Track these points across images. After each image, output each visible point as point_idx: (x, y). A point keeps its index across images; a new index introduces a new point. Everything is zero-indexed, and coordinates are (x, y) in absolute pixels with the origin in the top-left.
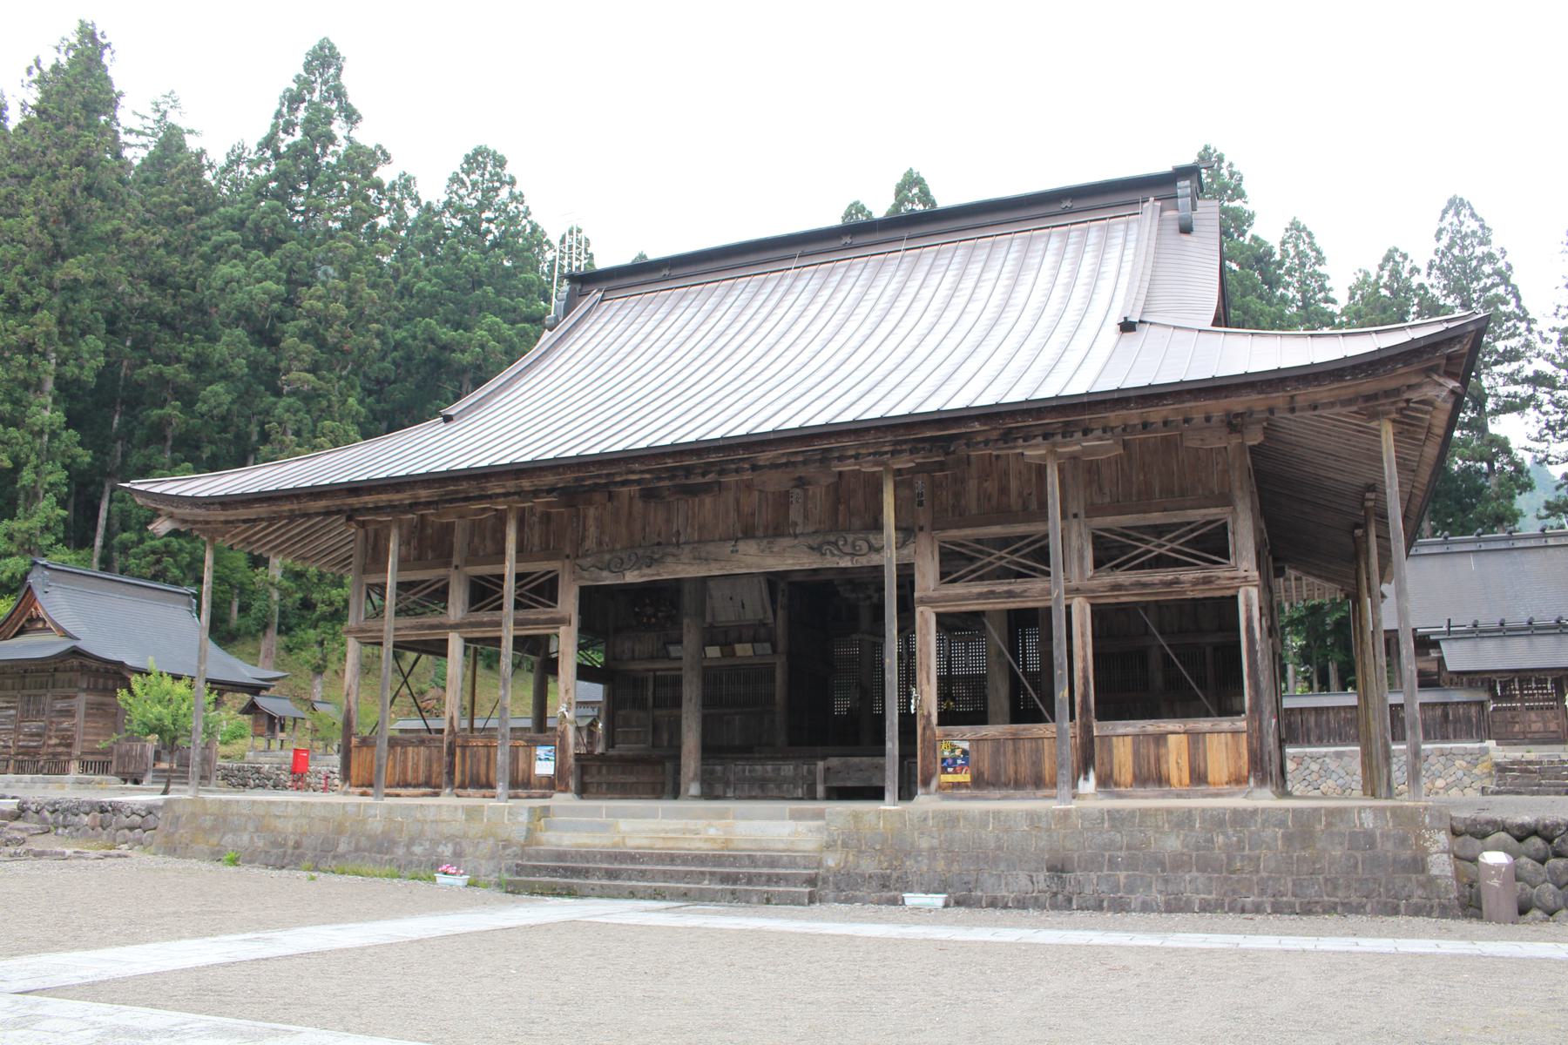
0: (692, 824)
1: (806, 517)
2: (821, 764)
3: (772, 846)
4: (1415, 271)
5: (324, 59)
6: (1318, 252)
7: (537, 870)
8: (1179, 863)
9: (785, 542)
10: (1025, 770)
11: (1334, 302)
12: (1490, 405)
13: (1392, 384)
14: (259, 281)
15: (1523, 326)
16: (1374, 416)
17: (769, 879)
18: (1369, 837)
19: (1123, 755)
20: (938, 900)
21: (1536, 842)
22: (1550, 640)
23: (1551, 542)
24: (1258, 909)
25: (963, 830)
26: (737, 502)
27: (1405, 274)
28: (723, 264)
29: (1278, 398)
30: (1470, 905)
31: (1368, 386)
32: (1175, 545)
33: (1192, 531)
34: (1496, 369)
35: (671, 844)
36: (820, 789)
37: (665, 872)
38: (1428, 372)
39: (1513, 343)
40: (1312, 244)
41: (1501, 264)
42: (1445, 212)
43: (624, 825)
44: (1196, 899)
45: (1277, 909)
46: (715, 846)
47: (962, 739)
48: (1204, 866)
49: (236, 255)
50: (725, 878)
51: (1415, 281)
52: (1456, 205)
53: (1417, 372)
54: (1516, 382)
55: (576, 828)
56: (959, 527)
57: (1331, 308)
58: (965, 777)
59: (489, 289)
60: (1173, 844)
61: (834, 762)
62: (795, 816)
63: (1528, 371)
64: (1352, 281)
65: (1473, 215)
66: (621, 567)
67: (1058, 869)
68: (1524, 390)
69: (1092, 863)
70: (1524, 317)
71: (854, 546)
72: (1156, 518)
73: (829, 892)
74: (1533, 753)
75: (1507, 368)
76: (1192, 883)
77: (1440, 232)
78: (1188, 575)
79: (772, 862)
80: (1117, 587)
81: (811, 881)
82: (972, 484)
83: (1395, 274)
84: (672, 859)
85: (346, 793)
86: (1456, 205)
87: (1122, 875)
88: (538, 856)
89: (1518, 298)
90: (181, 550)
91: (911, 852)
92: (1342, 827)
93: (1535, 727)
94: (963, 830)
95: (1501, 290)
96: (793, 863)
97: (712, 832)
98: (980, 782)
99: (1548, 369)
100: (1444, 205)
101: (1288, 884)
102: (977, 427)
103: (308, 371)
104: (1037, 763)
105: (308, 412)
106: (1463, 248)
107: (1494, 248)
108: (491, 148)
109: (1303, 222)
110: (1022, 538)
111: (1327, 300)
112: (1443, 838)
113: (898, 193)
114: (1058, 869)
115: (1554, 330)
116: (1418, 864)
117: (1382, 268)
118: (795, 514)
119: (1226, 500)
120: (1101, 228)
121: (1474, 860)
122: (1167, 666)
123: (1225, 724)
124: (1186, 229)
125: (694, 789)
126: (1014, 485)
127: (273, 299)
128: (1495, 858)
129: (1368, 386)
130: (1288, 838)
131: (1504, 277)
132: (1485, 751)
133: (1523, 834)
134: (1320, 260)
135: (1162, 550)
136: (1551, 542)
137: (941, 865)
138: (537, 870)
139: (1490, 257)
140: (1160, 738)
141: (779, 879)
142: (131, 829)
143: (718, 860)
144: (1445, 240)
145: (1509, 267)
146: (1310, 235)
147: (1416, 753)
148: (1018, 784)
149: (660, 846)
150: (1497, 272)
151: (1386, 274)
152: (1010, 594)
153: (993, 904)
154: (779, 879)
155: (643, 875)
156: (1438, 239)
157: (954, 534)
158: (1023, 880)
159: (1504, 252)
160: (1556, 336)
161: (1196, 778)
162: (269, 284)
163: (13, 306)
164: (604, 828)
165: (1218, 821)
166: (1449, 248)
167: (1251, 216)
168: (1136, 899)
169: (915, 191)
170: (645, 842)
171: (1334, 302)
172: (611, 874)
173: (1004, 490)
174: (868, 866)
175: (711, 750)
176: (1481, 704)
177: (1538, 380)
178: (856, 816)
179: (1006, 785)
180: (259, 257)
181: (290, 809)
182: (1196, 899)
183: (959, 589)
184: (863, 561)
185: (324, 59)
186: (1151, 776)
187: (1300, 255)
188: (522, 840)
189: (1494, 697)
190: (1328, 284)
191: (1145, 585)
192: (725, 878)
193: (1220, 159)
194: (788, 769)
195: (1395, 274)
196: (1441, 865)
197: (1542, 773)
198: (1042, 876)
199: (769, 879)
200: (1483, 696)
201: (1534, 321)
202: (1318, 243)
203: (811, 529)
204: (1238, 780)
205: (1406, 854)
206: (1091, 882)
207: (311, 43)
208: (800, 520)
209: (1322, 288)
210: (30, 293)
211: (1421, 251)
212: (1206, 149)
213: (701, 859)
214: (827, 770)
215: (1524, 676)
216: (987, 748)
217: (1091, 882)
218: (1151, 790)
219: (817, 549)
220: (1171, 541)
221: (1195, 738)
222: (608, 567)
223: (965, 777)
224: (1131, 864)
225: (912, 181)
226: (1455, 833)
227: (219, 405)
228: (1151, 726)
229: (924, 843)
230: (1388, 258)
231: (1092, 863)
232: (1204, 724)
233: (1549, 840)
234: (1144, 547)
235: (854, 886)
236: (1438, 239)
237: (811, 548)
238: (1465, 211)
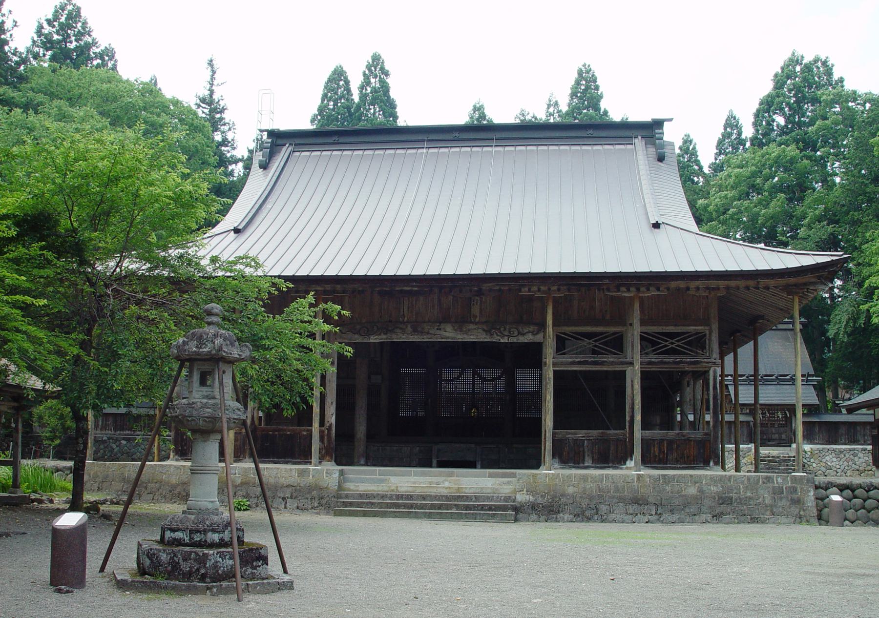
1: (481, 313)
3: (484, 491)
26: (439, 300)
28: (352, 139)
31: (793, 280)
32: (679, 344)
33: (689, 337)
35: (426, 490)
36: (435, 462)
37: (492, 501)
46: (452, 490)
53: (814, 277)
56: (567, 325)
62: (491, 476)
66: (368, 334)
71: (510, 332)
72: (671, 329)
85: (177, 460)
97: (447, 484)
102: (607, 281)
110: (602, 333)
118: (475, 310)
119: (706, 322)
122: (592, 418)
126: (597, 304)
129: (793, 280)
135: (673, 346)
147: (737, 450)
149: (418, 492)
155: (422, 507)
164: (382, 481)
170: (410, 489)
178: (534, 476)
181: (172, 469)
183: (567, 359)
184: (514, 340)
188: (336, 488)
191: (665, 363)
203: (483, 320)
208: (478, 314)
213: (448, 498)
220: (678, 341)
222: (358, 333)
225: (478, 109)
226: (817, 487)
233: (853, 491)
234: (679, 344)
237: (484, 330)
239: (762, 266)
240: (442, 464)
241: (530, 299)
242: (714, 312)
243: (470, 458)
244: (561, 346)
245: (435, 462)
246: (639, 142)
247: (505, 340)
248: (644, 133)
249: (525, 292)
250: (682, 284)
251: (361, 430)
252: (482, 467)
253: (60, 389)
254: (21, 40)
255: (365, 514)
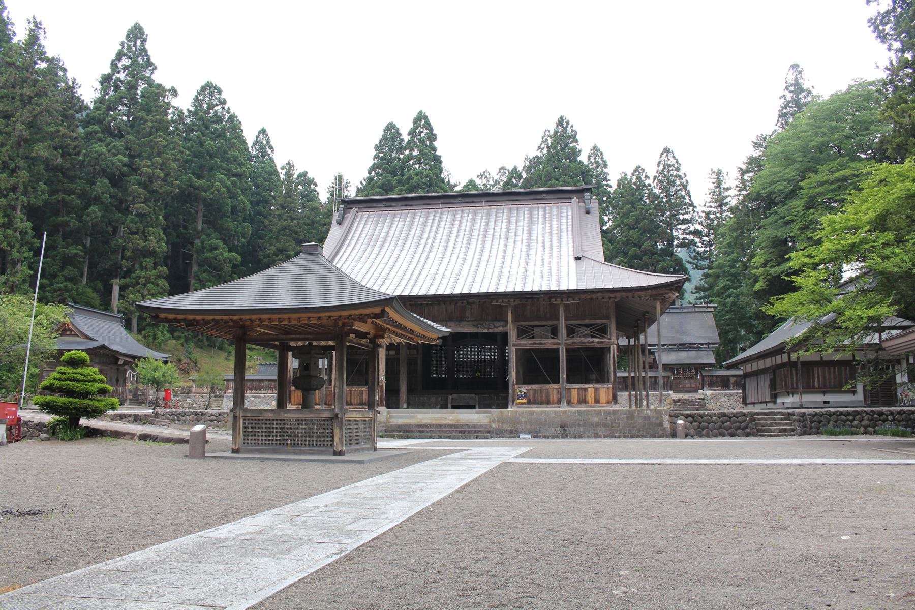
0: (444, 416)
2: (450, 397)
4: (647, 177)
5: (136, 33)
6: (605, 162)
7: (394, 431)
8: (598, 425)
9: (464, 323)
10: (544, 399)
11: (610, 187)
12: (675, 243)
13: (661, 292)
14: (115, 155)
15: (691, 208)
16: (655, 299)
17: (475, 431)
18: (649, 418)
19: (574, 394)
20: (530, 436)
21: (690, 418)
22: (694, 353)
23: (697, 310)
24: (619, 437)
25: (535, 416)
27: (643, 179)
29: (630, 295)
30: (674, 435)
31: (654, 292)
34: (679, 227)
36: (450, 406)
38: (671, 290)
39: (686, 217)
40: (602, 158)
41: (684, 180)
42: (662, 154)
43: (419, 416)
44: (602, 435)
45: (624, 437)
47: (524, 389)
48: (605, 425)
49: (100, 140)
50: (461, 431)
51: (647, 182)
52: (667, 151)
54: (686, 234)
55: (401, 418)
57: (609, 189)
58: (525, 401)
59: (218, 160)
60: (596, 419)
61: (455, 396)
63: (692, 229)
64: (619, 177)
65: (674, 157)
67: (563, 427)
68: (691, 237)
69: (573, 425)
70: (691, 205)
73: (494, 435)
74: (686, 396)
75: (683, 227)
76: (601, 430)
77: (659, 163)
78: (596, 340)
79: (475, 426)
80: (574, 343)
81: (489, 432)
82: (528, 307)
83: (639, 178)
84: (441, 426)
86: (667, 151)
87: (582, 429)
88: (391, 426)
89: (690, 197)
90: (72, 289)
91: (519, 423)
92: (641, 415)
93: (688, 386)
94: (535, 416)
95: (683, 193)
96: (481, 426)
98: (529, 402)
99: (699, 227)
100: (662, 151)
101: (627, 430)
103: (143, 203)
104: (548, 397)
105: (141, 222)
106: (669, 171)
107: (681, 173)
108: (214, 83)
109: (599, 147)
111: (608, 185)
112: (667, 417)
113: (415, 122)
114: (563, 427)
115: (703, 212)
116: (661, 424)
117: (633, 175)
118: (468, 314)
119: (608, 318)
120: (558, 207)
121: (675, 423)
122: (588, 366)
123: (605, 386)
124: (588, 212)
125: (405, 405)
126: (542, 308)
127: (125, 165)
128: (680, 422)
130: (627, 418)
131: (685, 186)
132: (669, 395)
133: (687, 416)
134: (605, 166)
136: (697, 310)
137: (528, 426)
138: (394, 431)
139: (680, 178)
140: (586, 390)
141: (478, 431)
142: (212, 421)
143: (456, 426)
144: (661, 167)
145: (687, 182)
146: (601, 153)
148: (541, 403)
149: (438, 422)
150: (682, 184)
151: (635, 177)
152: (541, 344)
153: (544, 437)
154: (478, 431)
155: (432, 431)
156: (658, 166)
157: (523, 323)
158: (553, 430)
159: (685, 174)
160: (703, 215)
161: (598, 400)
162: (120, 157)
163: (5, 166)
164: (412, 417)
165: (608, 413)
166: (663, 171)
167: (580, 151)
168: (586, 435)
169: (423, 122)
171: (610, 187)
172: (421, 431)
173: (539, 310)
174: (506, 427)
175: (410, 391)
176: (669, 377)
177: (696, 233)
179: (538, 403)
180: (112, 142)
182: (602, 435)
183: (523, 341)
184: (492, 331)
185: (136, 33)
186: (583, 401)
187: (597, 163)
189: (674, 374)
190: (608, 178)
192: (461, 431)
193: (568, 123)
194: (433, 399)
195: (639, 178)
196: (667, 424)
197: (689, 403)
198: (559, 429)
199: (475, 431)
200: (669, 374)
201: (696, 207)
202: (605, 158)
204: (608, 402)
205: (658, 422)
206: (573, 430)
207: (129, 26)
209: (606, 179)
210: (14, 161)
211: (651, 171)
212: (561, 117)
213: (450, 426)
214: (175, 396)
215: (684, 366)
216: (532, 392)
217: (573, 430)
218: (583, 405)
219: (476, 326)
221: (596, 389)
223: (525, 401)
224: (584, 425)
226: (671, 416)
227: (96, 217)
228: (583, 386)
229: (523, 420)
230: (635, 171)
231: (573, 425)
232: (599, 386)
235: (502, 433)
236: (658, 166)
238: (670, 155)
239: (635, 284)
240: (454, 407)
241: (500, 306)
242: (612, 312)
243: (471, 403)
244: (521, 333)
245: (450, 406)
246: (575, 200)
247: (486, 331)
248: (579, 195)
249: (494, 302)
250: (588, 296)
251: (403, 388)
252: (480, 408)
253: (282, 177)
254: (89, 93)
255: (449, 437)
